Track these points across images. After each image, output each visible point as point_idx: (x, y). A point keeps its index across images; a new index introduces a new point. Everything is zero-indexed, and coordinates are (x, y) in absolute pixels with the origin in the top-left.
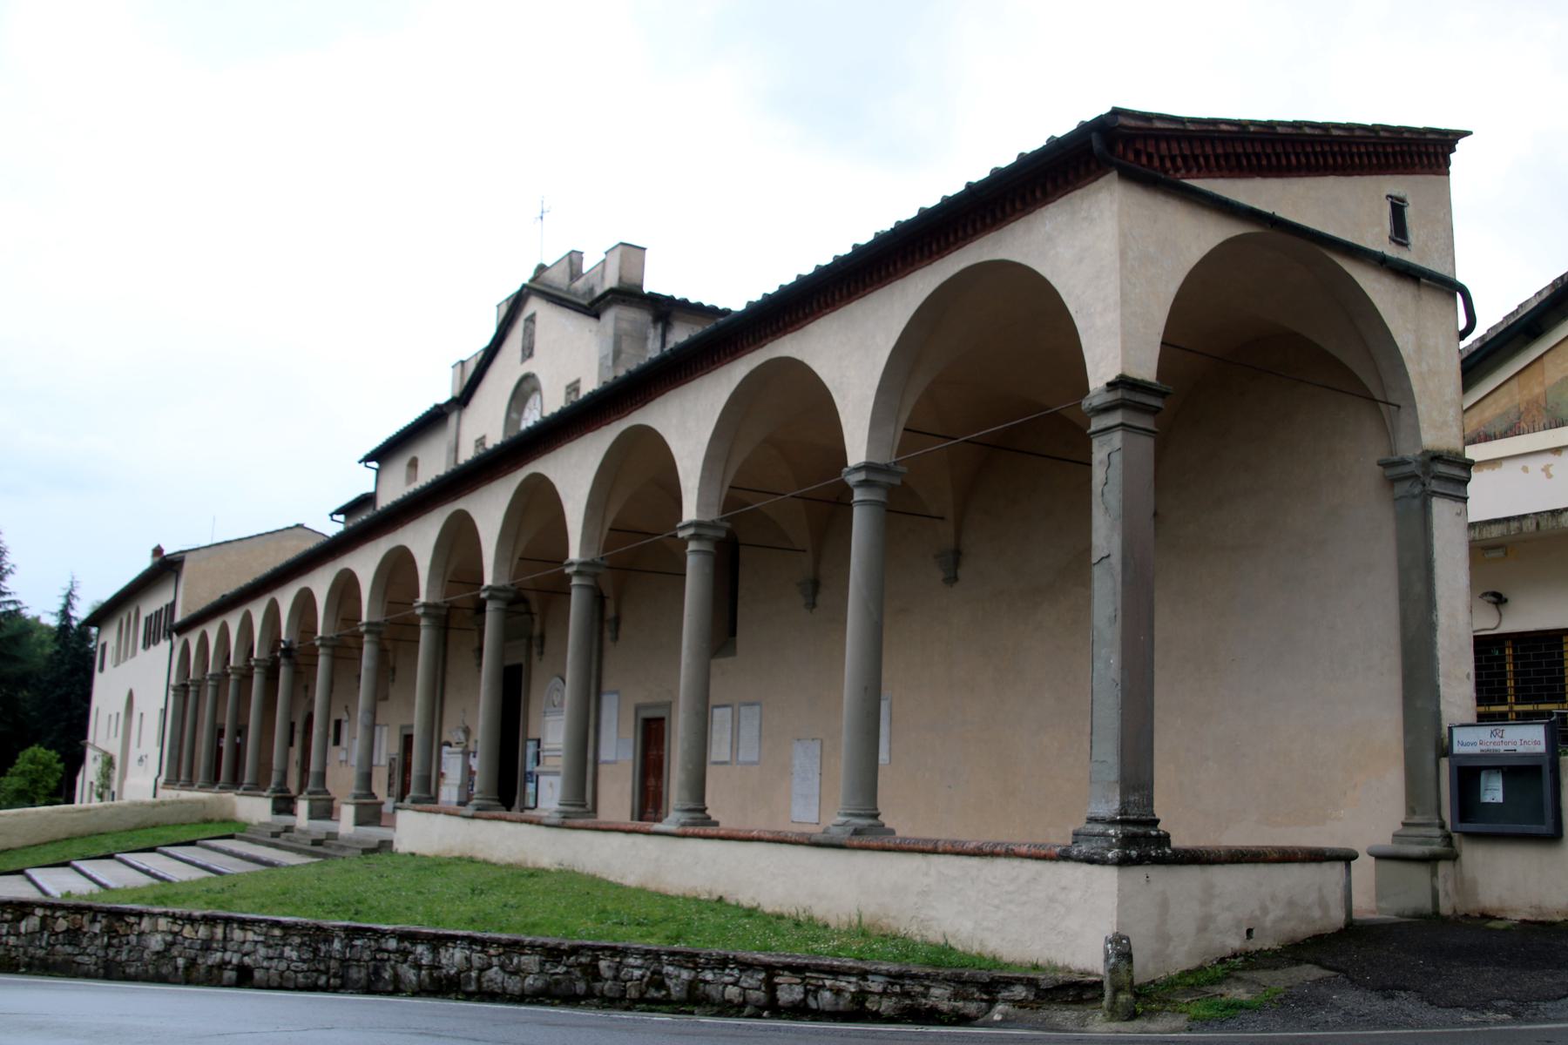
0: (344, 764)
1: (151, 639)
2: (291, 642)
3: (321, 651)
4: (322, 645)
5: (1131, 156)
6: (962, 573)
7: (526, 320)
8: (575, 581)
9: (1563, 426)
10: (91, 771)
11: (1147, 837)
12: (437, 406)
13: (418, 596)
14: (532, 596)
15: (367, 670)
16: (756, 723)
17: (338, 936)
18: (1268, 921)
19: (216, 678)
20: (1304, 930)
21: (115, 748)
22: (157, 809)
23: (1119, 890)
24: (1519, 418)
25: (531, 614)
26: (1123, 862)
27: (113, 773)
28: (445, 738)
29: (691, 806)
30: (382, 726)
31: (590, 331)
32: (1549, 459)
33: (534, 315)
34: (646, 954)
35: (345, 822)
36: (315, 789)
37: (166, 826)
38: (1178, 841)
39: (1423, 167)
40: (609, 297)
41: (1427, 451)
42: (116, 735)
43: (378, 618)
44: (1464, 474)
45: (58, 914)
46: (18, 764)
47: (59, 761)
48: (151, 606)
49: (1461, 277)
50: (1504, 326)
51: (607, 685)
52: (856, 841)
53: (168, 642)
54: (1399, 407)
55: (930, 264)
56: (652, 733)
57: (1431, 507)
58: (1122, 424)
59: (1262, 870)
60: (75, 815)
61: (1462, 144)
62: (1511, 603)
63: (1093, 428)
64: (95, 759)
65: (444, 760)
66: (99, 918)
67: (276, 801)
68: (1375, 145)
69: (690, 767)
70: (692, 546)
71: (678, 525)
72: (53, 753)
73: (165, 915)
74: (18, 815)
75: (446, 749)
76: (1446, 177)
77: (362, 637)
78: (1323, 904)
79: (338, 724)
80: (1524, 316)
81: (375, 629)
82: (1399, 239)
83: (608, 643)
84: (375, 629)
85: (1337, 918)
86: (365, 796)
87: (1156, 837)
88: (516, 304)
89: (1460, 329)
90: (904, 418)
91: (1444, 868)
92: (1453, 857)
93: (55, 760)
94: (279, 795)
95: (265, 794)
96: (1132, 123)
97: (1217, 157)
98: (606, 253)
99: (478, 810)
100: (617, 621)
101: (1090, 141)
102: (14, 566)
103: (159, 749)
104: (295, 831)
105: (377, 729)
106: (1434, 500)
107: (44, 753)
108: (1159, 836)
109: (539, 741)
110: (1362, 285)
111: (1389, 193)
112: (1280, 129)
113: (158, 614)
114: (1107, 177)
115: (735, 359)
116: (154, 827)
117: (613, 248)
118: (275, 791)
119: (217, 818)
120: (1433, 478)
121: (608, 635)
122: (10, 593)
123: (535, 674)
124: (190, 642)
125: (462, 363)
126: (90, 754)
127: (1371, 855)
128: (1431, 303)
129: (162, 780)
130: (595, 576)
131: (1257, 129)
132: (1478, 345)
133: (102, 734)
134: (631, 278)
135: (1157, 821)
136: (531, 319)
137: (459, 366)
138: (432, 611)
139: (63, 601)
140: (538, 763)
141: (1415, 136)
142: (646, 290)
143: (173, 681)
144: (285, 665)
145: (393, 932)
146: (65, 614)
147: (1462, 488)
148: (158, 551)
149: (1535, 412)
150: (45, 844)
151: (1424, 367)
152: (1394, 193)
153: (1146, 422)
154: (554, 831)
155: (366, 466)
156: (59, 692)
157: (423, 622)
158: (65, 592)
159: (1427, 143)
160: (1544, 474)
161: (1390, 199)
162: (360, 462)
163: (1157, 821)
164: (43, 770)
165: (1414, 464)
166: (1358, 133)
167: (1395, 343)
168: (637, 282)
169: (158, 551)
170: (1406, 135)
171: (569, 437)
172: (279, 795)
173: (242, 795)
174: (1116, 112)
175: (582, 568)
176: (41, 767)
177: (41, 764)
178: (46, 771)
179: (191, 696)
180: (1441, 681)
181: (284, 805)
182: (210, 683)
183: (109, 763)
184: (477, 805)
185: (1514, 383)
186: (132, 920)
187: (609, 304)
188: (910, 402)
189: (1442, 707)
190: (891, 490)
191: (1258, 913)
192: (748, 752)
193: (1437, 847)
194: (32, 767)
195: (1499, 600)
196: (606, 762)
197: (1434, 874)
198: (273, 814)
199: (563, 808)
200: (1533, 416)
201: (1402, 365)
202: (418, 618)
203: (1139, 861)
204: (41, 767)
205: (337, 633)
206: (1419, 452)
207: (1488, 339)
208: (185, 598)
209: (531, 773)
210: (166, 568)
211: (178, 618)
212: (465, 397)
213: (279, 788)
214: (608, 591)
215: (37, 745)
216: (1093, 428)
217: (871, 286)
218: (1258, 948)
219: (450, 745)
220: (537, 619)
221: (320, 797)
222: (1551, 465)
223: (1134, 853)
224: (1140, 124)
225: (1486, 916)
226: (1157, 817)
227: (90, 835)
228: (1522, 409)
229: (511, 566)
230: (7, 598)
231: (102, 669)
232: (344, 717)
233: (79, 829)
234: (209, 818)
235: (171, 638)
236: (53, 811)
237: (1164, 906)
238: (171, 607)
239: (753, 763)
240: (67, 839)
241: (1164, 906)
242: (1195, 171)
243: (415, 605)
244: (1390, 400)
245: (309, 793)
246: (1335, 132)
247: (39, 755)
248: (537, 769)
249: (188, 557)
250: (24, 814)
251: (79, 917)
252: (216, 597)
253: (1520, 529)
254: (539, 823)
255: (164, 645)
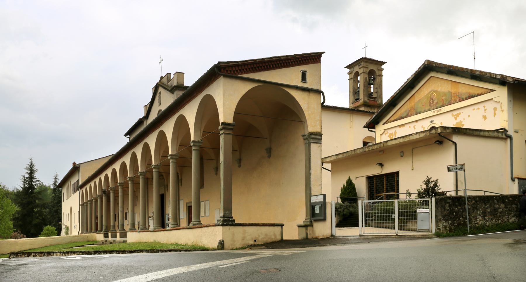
0: (128, 225)
1: (74, 191)
2: (105, 189)
3: (111, 191)
4: (111, 190)
5: (225, 72)
6: (242, 164)
7: (159, 93)
8: (154, 170)
9: (419, 114)
10: (64, 230)
11: (229, 220)
12: (140, 119)
13: (128, 175)
14: (164, 174)
15: (120, 196)
16: (208, 206)
17: (93, 253)
18: (260, 238)
19: (90, 201)
20: (270, 241)
21: (69, 225)
22: (74, 238)
23: (222, 231)
24: (409, 112)
25: (164, 179)
26: (223, 225)
27: (69, 232)
28: (149, 215)
29: (174, 223)
30: (136, 213)
31: (172, 98)
32: (415, 124)
33: (160, 92)
34: (146, 251)
35: (118, 239)
36: (112, 230)
37: (77, 242)
38: (236, 222)
39: (312, 62)
40: (174, 88)
41: (310, 132)
42: (69, 221)
43: (122, 182)
44: (320, 137)
45: (37, 254)
46: (44, 231)
47: (56, 230)
48: (73, 180)
49: (322, 90)
50: (404, 86)
51: (181, 198)
52: (195, 226)
53: (78, 191)
54: (304, 122)
55: (200, 94)
56: (189, 209)
57: (310, 146)
58: (223, 133)
59: (258, 227)
60: (51, 239)
61: (323, 55)
62: (385, 166)
63: (220, 133)
64: (64, 228)
65: (149, 222)
66: (45, 254)
67: (104, 234)
68: (296, 59)
69: (173, 214)
70: (171, 161)
71: (168, 155)
72: (54, 227)
73: (59, 252)
74: (36, 239)
75: (150, 218)
76: (320, 64)
77: (118, 187)
78: (275, 235)
79: (126, 213)
80: (409, 82)
81: (121, 185)
82: (303, 81)
83: (180, 186)
84: (121, 185)
85: (279, 238)
86: (122, 230)
87: (231, 220)
88: (156, 88)
89: (322, 102)
90: (202, 130)
91: (309, 228)
92: (312, 226)
93: (54, 230)
94: (105, 232)
95: (102, 233)
96: (224, 65)
97: (249, 69)
98: (174, 75)
99: (141, 230)
100: (181, 180)
101: (215, 70)
102: (37, 169)
103: (79, 223)
104: (108, 241)
105: (135, 214)
106: (311, 144)
107: (51, 228)
108: (232, 220)
109: (168, 214)
110: (292, 94)
111: (301, 70)
112: (266, 60)
113: (75, 183)
114: (220, 78)
115: (175, 114)
116: (73, 243)
117: (175, 73)
118: (104, 232)
119: (91, 240)
120: (311, 139)
121: (180, 184)
122: (37, 178)
123: (166, 195)
124: (83, 191)
125: (146, 106)
126: (63, 227)
127: (298, 226)
128: (313, 96)
129: (80, 232)
130: (159, 168)
131: (259, 61)
132: (398, 91)
133: (65, 221)
134: (180, 82)
135: (233, 217)
136: (160, 93)
137: (145, 106)
138: (131, 179)
139: (54, 180)
140: (168, 220)
141: (307, 55)
142: (185, 85)
143: (80, 203)
144: (104, 196)
145: (102, 251)
146: (55, 184)
147: (320, 141)
148: (74, 164)
149: (412, 111)
150: (44, 247)
151: (310, 112)
152: (303, 70)
153: (231, 132)
154: (153, 233)
155: (126, 137)
156: (54, 209)
157: (129, 182)
158: (54, 178)
159: (312, 56)
160: (414, 128)
161: (302, 72)
162: (124, 136)
163: (233, 217)
164: (51, 233)
165: (307, 136)
166: (289, 57)
167: (301, 107)
168: (182, 83)
169: (74, 164)
170: (304, 55)
171: (150, 133)
172: (105, 232)
173: (97, 234)
174: (219, 63)
175: (155, 167)
176: (50, 232)
177: (50, 231)
178: (52, 233)
179: (85, 207)
180: (312, 186)
181: (106, 236)
182: (89, 203)
183: (67, 228)
184: (141, 229)
185: (408, 102)
186: (52, 254)
187: (175, 90)
188: (203, 125)
189: (312, 192)
190: (200, 147)
191: (257, 236)
192: (207, 214)
193: (309, 223)
194: (48, 232)
195: (381, 165)
196: (182, 219)
197: (307, 229)
198: (104, 238)
199: (154, 227)
200: (412, 111)
201: (303, 112)
202: (128, 181)
203: (227, 225)
204: (50, 232)
205: (115, 186)
206: (308, 133)
207: (400, 90)
208: (81, 177)
209: (167, 223)
210: (76, 169)
211: (80, 184)
212: (147, 116)
213: (105, 231)
214: (179, 173)
215: (49, 225)
216: (220, 133)
217: (192, 98)
218: (257, 244)
219: (150, 217)
220: (166, 180)
221: (114, 232)
222: (415, 126)
223: (225, 223)
224: (226, 64)
225: (316, 238)
226: (233, 216)
227: (56, 245)
228: (410, 110)
229: (145, 166)
230: (36, 180)
231: (64, 201)
232: (127, 212)
233: (53, 243)
234: (89, 240)
235: (79, 190)
236: (45, 238)
237: (233, 234)
238: (78, 181)
239: (208, 216)
240: (50, 246)
241: (233, 234)
242: (243, 73)
243: (127, 177)
244: (302, 121)
245: (111, 231)
246: (282, 58)
247: (50, 228)
248: (168, 222)
249: (81, 165)
250: (37, 239)
251: (41, 255)
252: (458, 180)
253: (380, 146)
254: (150, 231)
255: (78, 192)
